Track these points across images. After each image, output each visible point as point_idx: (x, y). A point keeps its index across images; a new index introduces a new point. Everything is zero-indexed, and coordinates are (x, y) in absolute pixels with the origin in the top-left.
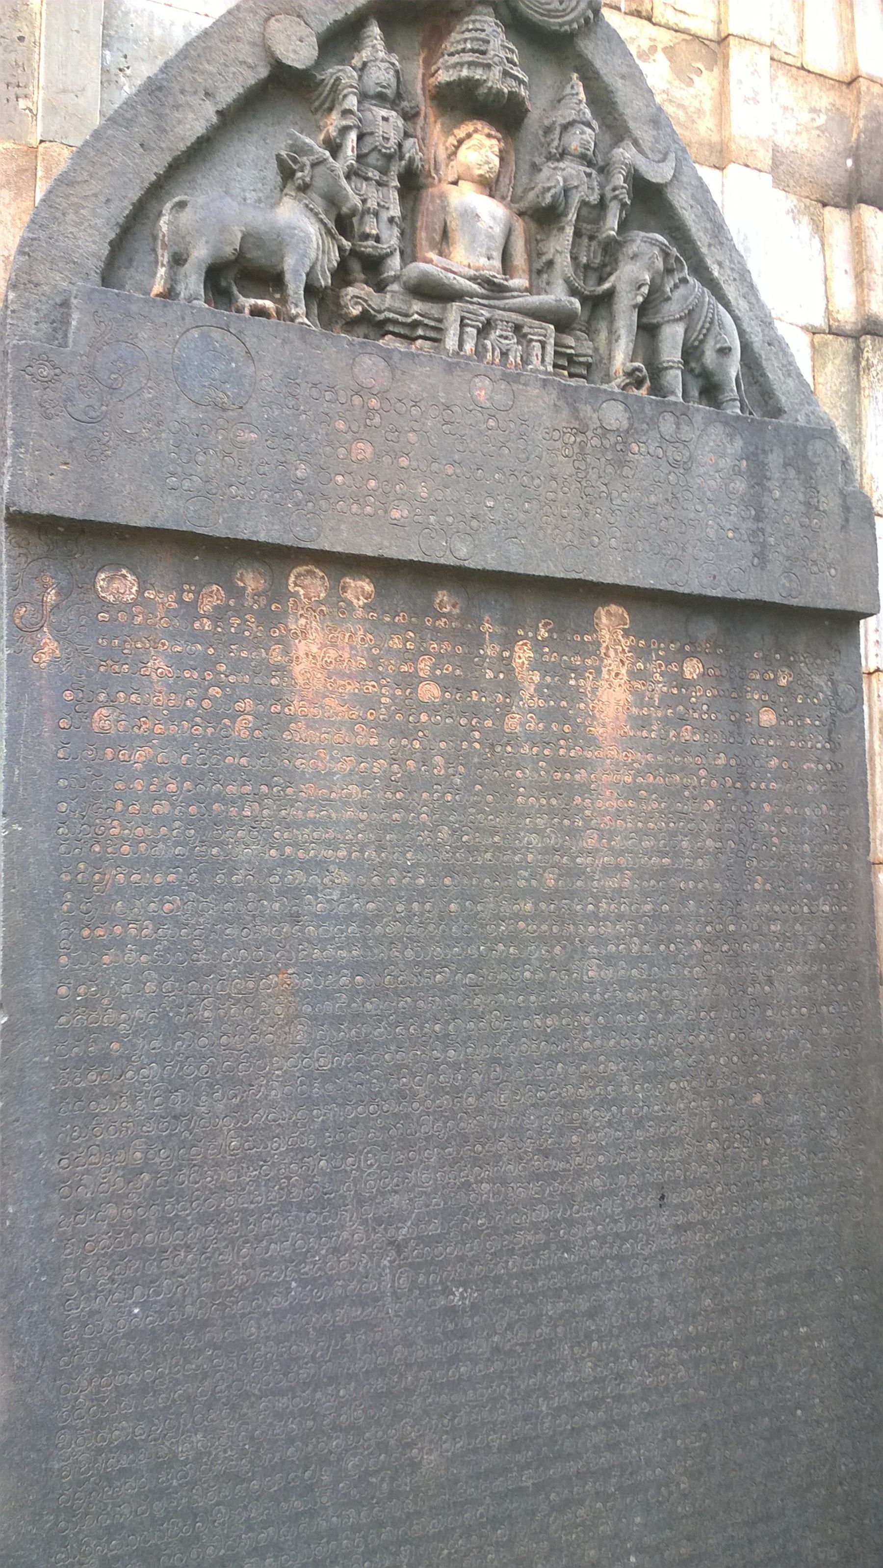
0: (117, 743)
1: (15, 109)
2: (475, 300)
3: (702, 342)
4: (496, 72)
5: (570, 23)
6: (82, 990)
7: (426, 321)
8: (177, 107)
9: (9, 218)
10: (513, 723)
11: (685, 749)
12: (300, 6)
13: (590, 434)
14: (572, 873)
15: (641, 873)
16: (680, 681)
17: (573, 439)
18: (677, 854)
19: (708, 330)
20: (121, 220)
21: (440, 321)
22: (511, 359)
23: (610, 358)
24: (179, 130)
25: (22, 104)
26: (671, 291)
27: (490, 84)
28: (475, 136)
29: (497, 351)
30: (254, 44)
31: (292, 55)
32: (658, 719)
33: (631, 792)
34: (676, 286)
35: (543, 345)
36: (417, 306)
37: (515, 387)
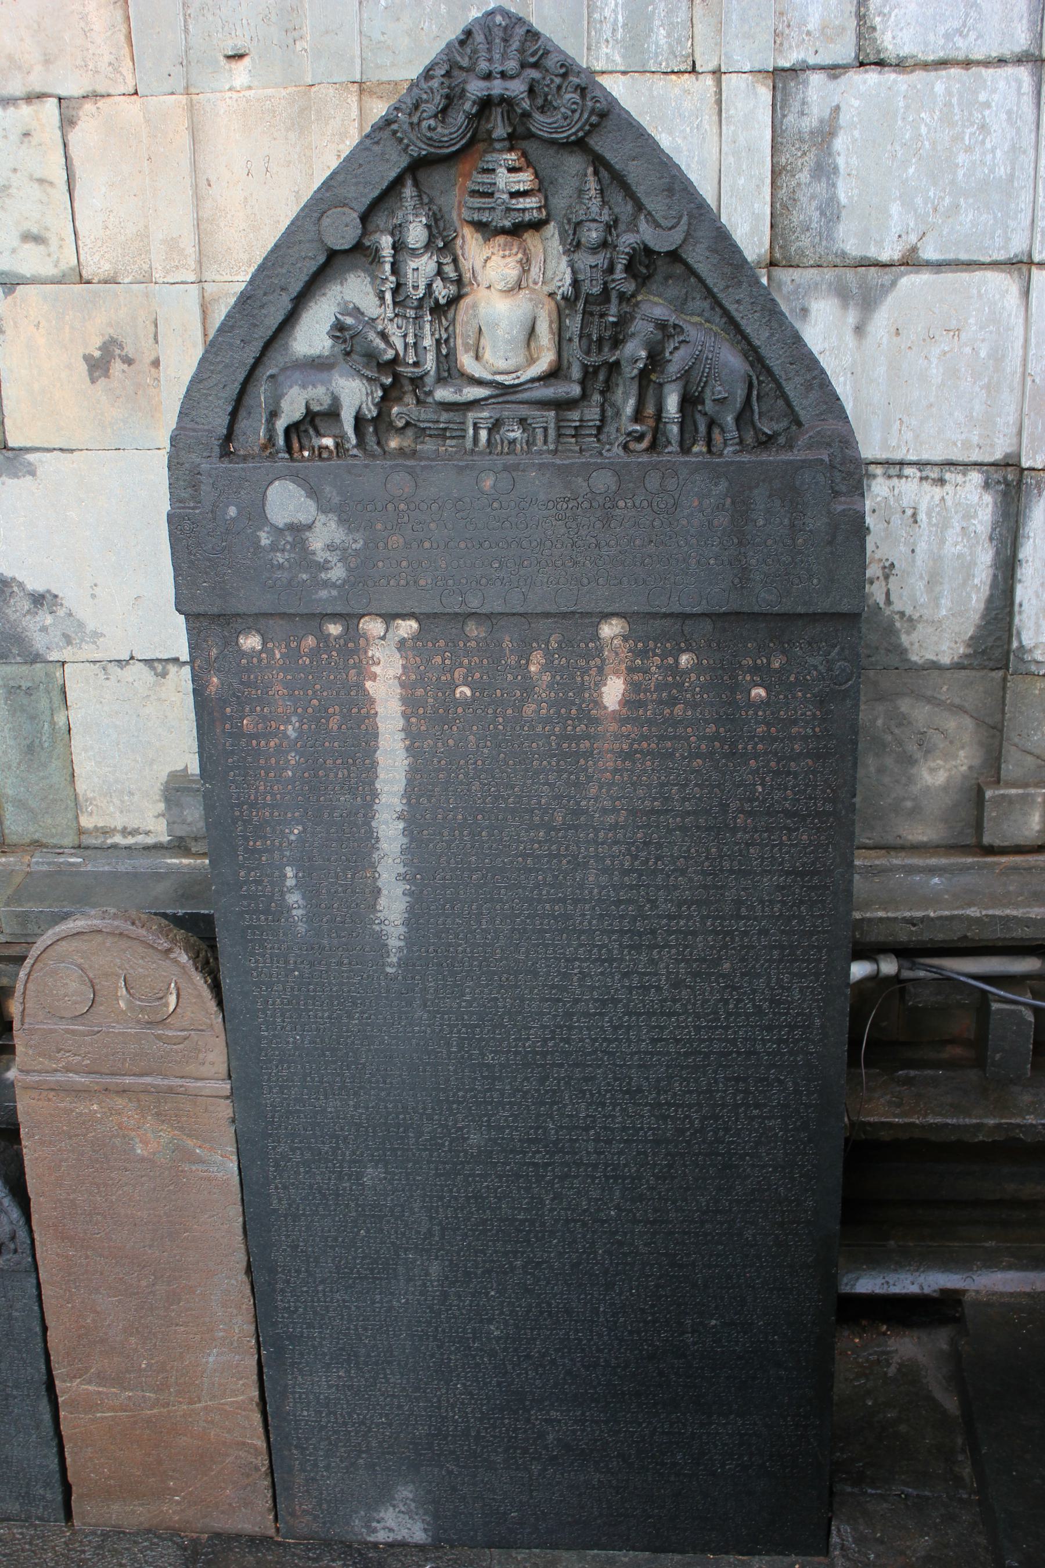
0: (255, 736)
3: (702, 391)
4: (499, 212)
8: (262, 307)
10: (529, 709)
11: (675, 723)
15: (633, 812)
16: (675, 669)
24: (267, 322)
25: (299, 46)
28: (494, 258)
32: (652, 701)
33: (628, 756)
34: (676, 348)
35: (546, 429)
37: (514, 474)
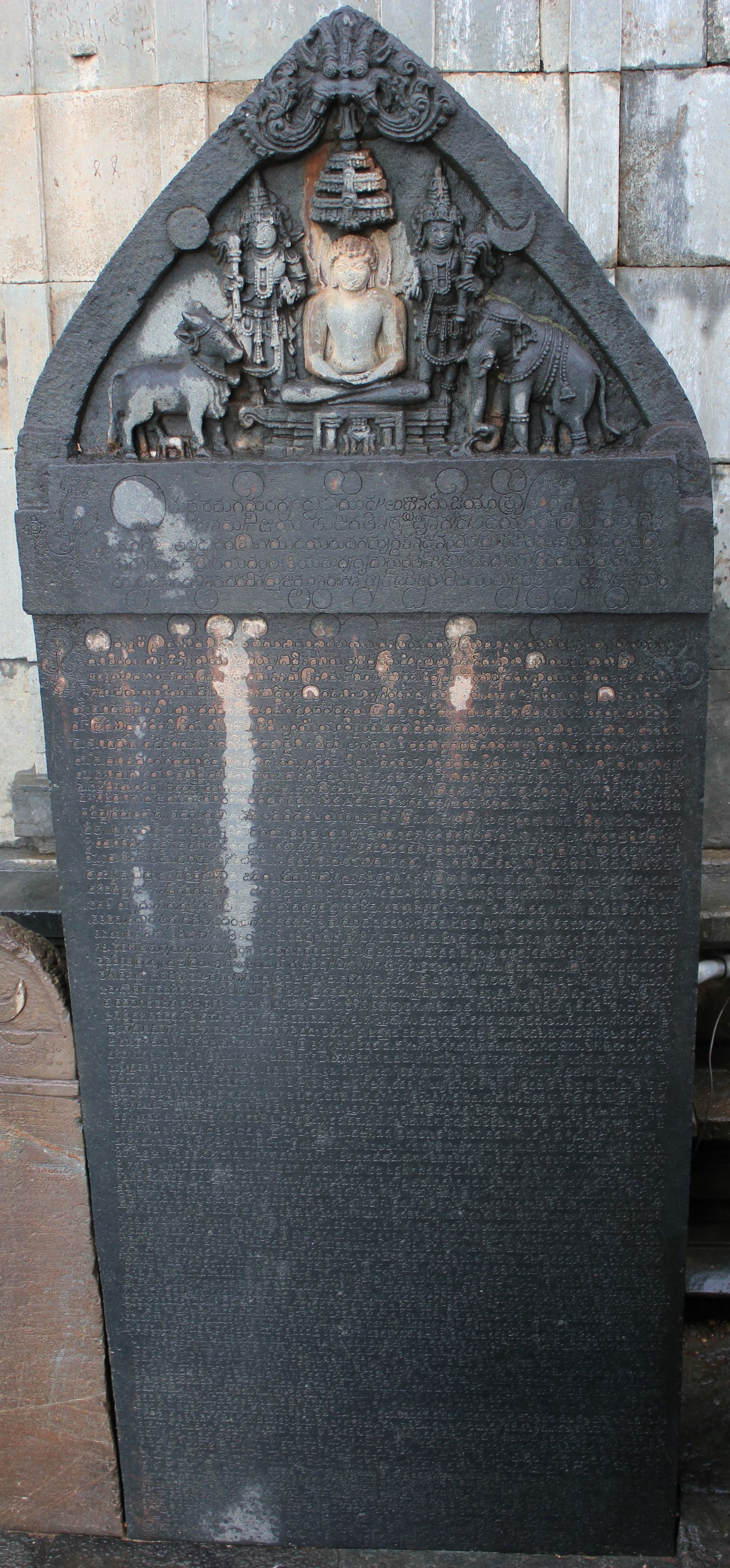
1: (141, 52)
2: (338, 401)
3: (550, 391)
4: (346, 212)
5: (423, 133)
6: (100, 873)
7: (299, 426)
8: (110, 307)
9: (144, 156)
10: (377, 710)
12: (193, 198)
13: (428, 500)
14: (425, 812)
17: (413, 506)
18: (514, 799)
19: (553, 383)
20: (82, 397)
21: (311, 423)
22: (366, 446)
23: (471, 408)
26: (519, 353)
27: (342, 224)
29: (354, 442)
30: (159, 241)
31: (189, 241)
34: (523, 348)
35: (393, 429)
36: (292, 416)
37: (362, 474)
